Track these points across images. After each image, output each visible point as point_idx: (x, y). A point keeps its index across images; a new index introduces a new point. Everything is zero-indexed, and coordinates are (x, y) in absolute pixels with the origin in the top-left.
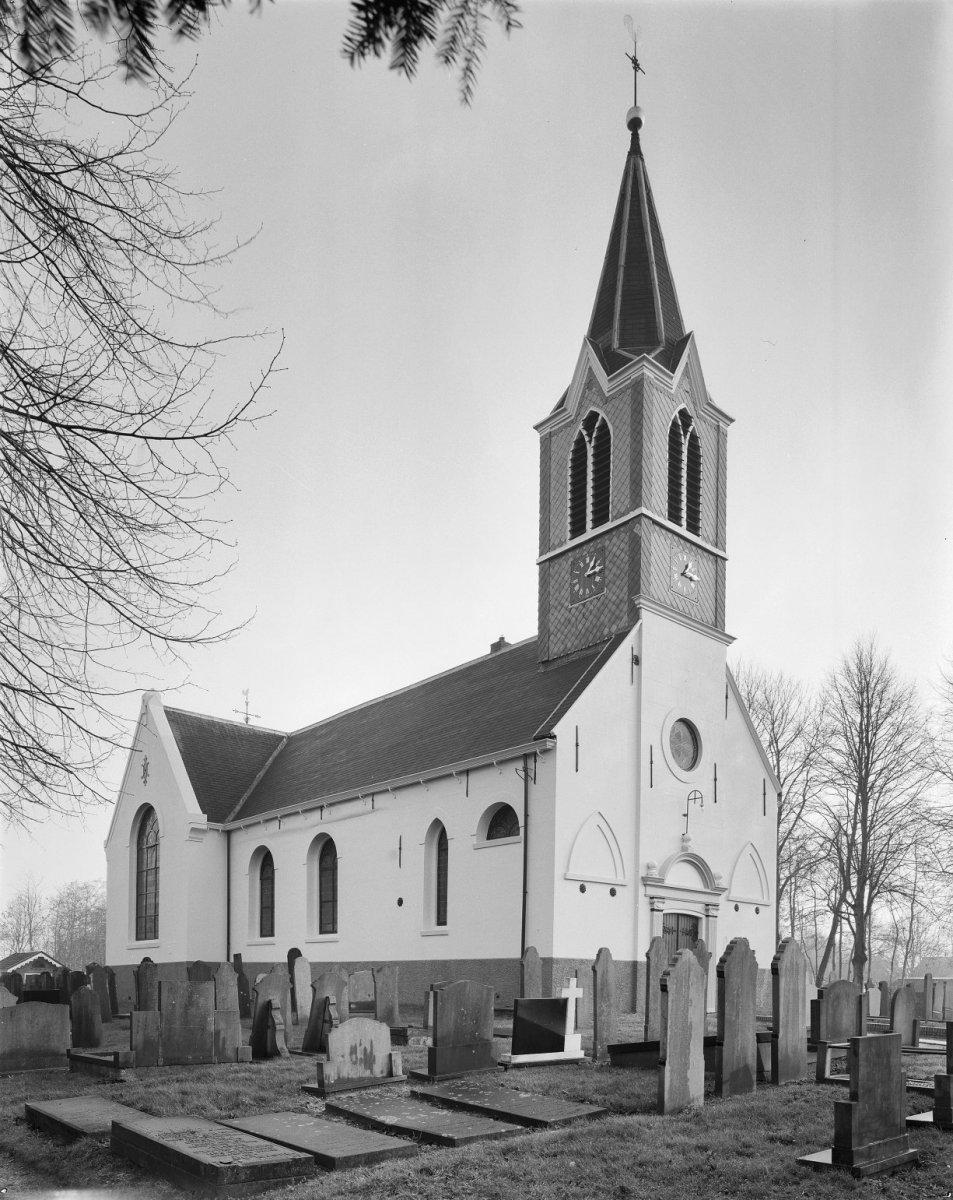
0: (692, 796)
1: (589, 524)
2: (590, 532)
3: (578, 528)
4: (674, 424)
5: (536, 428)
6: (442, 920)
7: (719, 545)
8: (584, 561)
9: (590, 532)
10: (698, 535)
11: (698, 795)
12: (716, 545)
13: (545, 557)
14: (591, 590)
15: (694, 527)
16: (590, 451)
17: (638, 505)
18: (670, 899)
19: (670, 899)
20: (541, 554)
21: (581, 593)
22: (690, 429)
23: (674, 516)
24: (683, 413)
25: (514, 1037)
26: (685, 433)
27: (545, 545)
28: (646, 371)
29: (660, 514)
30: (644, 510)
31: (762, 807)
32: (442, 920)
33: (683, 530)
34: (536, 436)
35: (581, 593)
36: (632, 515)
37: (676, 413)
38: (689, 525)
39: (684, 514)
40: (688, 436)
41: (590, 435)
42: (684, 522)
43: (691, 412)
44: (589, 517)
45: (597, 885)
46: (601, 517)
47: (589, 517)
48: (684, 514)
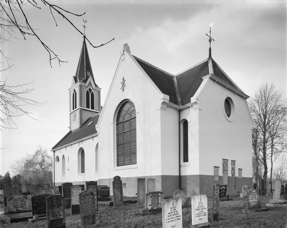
1: (75, 108)
2: (75, 110)
3: (73, 109)
4: (88, 91)
22: (91, 92)
23: (88, 107)
26: (90, 92)
40: (91, 93)
46: (76, 108)
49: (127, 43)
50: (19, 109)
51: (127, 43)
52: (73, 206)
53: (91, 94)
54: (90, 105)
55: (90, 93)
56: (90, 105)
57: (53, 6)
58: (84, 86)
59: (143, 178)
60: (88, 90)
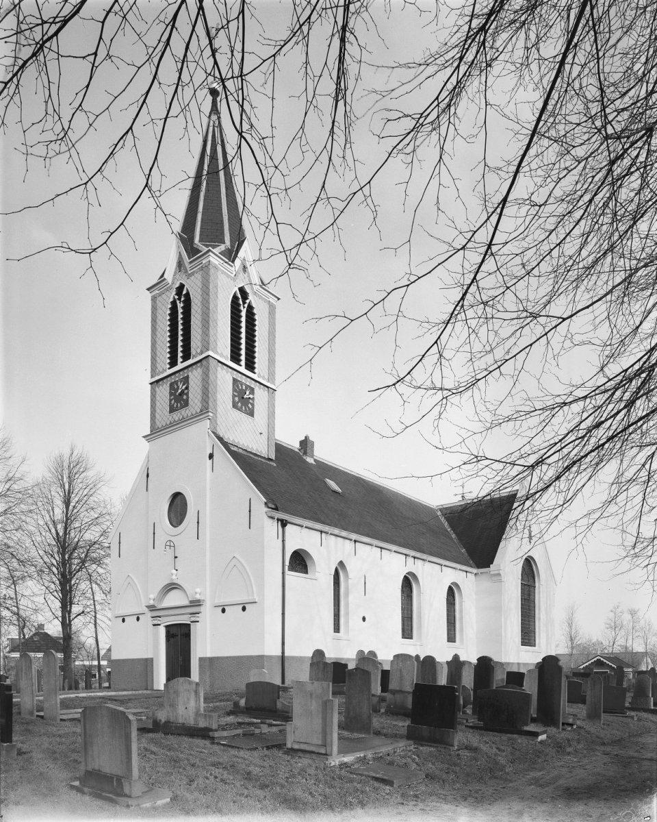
0: (168, 544)
1: (180, 360)
2: (180, 366)
3: (173, 363)
4: (235, 298)
5: (148, 289)
6: (337, 629)
7: (270, 381)
8: (177, 385)
9: (180, 366)
10: (255, 373)
11: (172, 544)
12: (269, 381)
13: (154, 380)
14: (181, 404)
15: (250, 366)
16: (180, 311)
17: (208, 350)
18: (163, 616)
19: (163, 616)
20: (152, 377)
21: (175, 406)
22: (248, 301)
23: (235, 357)
24: (242, 290)
25: (413, 695)
26: (244, 303)
27: (154, 371)
28: (211, 259)
29: (226, 358)
30: (210, 353)
31: (118, 553)
32: (337, 629)
33: (242, 369)
34: (149, 295)
35: (175, 406)
36: (204, 355)
37: (236, 289)
38: (246, 364)
39: (243, 358)
40: (246, 305)
41: (179, 299)
42: (243, 363)
43: (248, 290)
44: (180, 354)
45: (235, 606)
46: (187, 356)
47: (180, 354)
48: (243, 358)
49: (448, 641)
50: (637, 83)
51: (448, 641)
52: (209, 664)
53: (245, 309)
54: (243, 352)
55: (244, 307)
56: (243, 352)
57: (238, 127)
58: (223, 272)
59: (343, 662)
60: (235, 293)
